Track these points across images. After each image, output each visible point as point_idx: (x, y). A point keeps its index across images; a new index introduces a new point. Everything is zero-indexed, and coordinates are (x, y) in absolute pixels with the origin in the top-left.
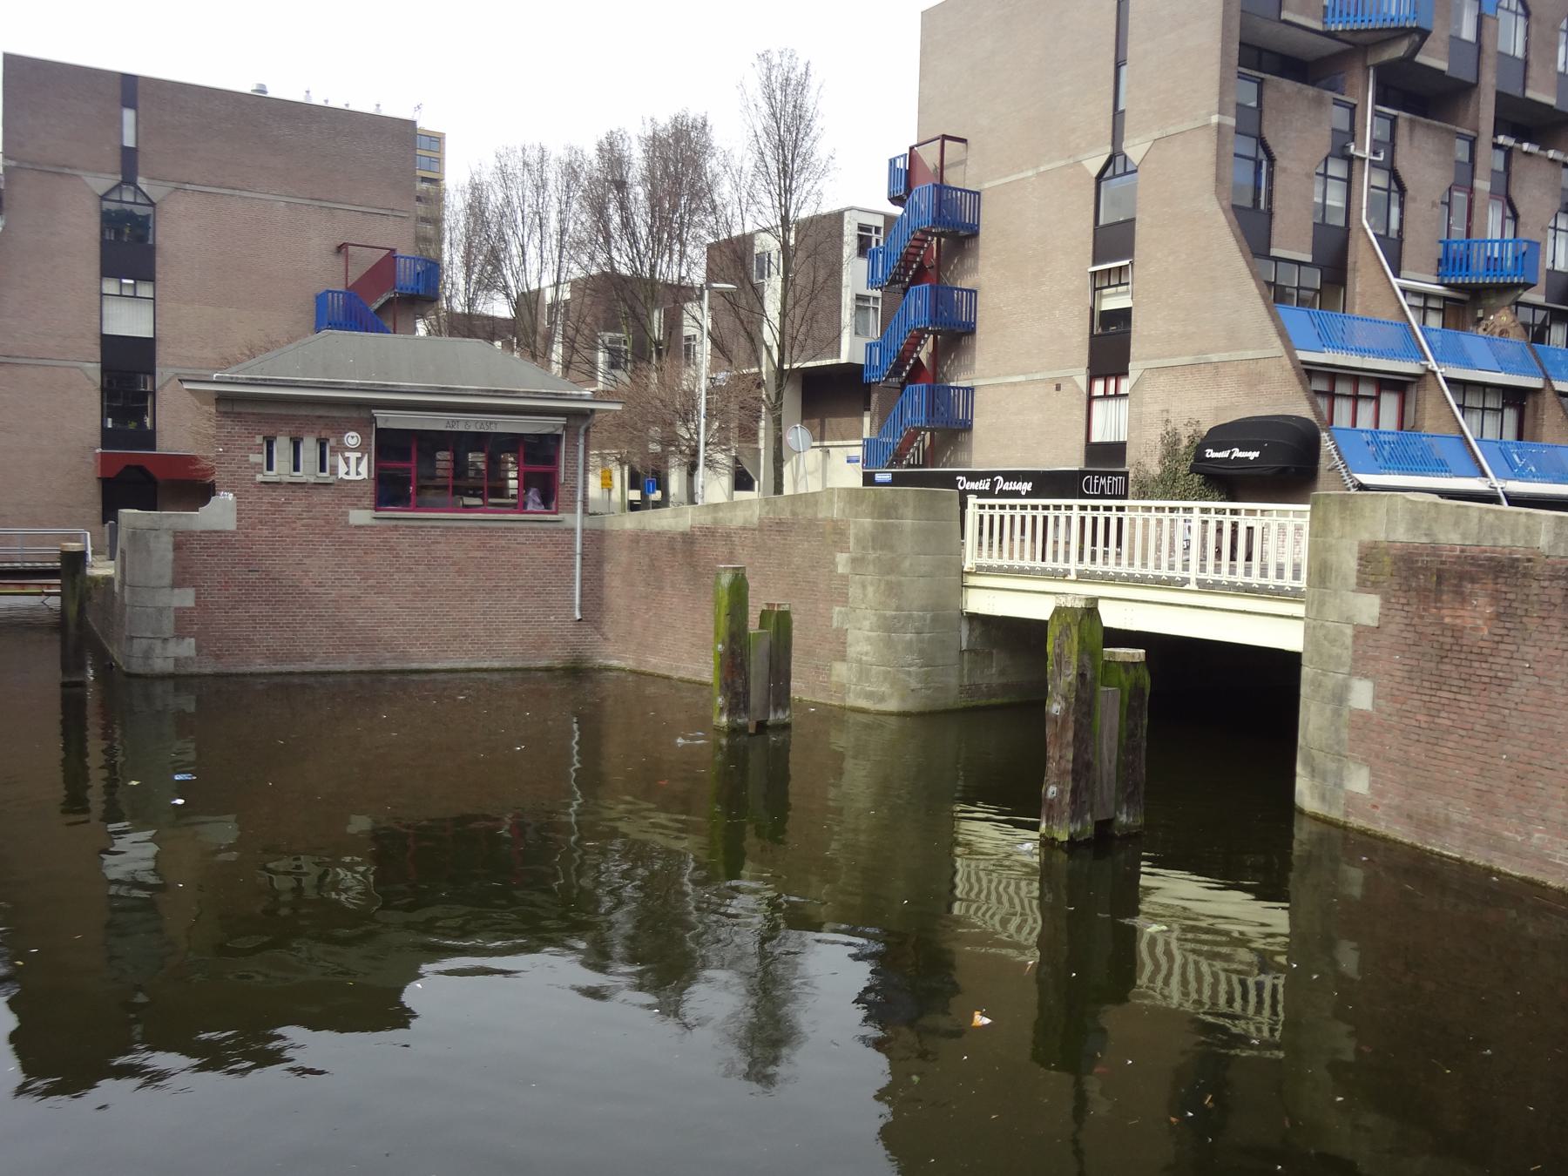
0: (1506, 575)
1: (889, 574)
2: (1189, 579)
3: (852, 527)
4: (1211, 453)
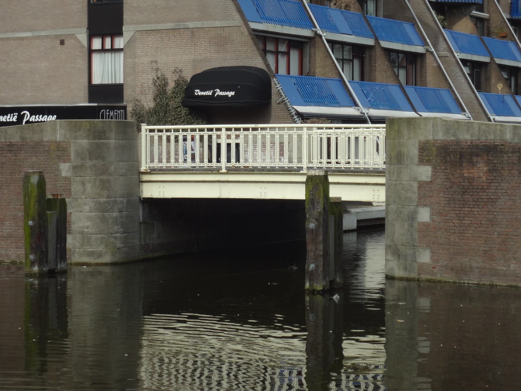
0: (492, 152)
1: (101, 175)
2: (302, 168)
3: (72, 145)
4: (198, 92)
